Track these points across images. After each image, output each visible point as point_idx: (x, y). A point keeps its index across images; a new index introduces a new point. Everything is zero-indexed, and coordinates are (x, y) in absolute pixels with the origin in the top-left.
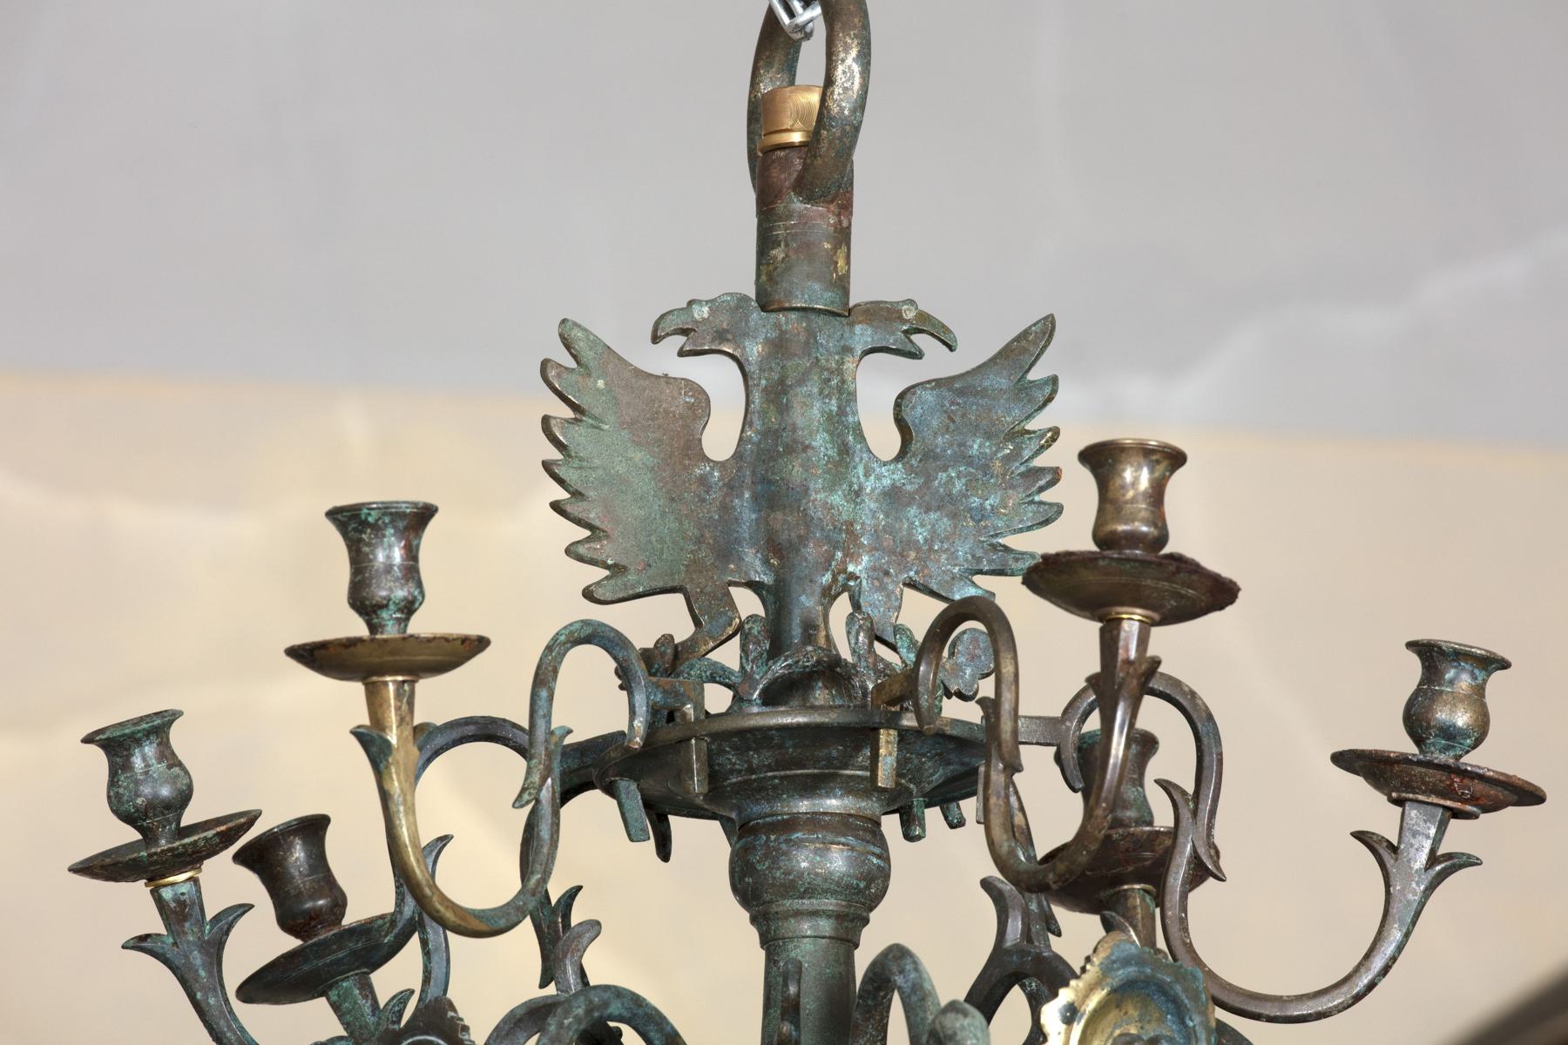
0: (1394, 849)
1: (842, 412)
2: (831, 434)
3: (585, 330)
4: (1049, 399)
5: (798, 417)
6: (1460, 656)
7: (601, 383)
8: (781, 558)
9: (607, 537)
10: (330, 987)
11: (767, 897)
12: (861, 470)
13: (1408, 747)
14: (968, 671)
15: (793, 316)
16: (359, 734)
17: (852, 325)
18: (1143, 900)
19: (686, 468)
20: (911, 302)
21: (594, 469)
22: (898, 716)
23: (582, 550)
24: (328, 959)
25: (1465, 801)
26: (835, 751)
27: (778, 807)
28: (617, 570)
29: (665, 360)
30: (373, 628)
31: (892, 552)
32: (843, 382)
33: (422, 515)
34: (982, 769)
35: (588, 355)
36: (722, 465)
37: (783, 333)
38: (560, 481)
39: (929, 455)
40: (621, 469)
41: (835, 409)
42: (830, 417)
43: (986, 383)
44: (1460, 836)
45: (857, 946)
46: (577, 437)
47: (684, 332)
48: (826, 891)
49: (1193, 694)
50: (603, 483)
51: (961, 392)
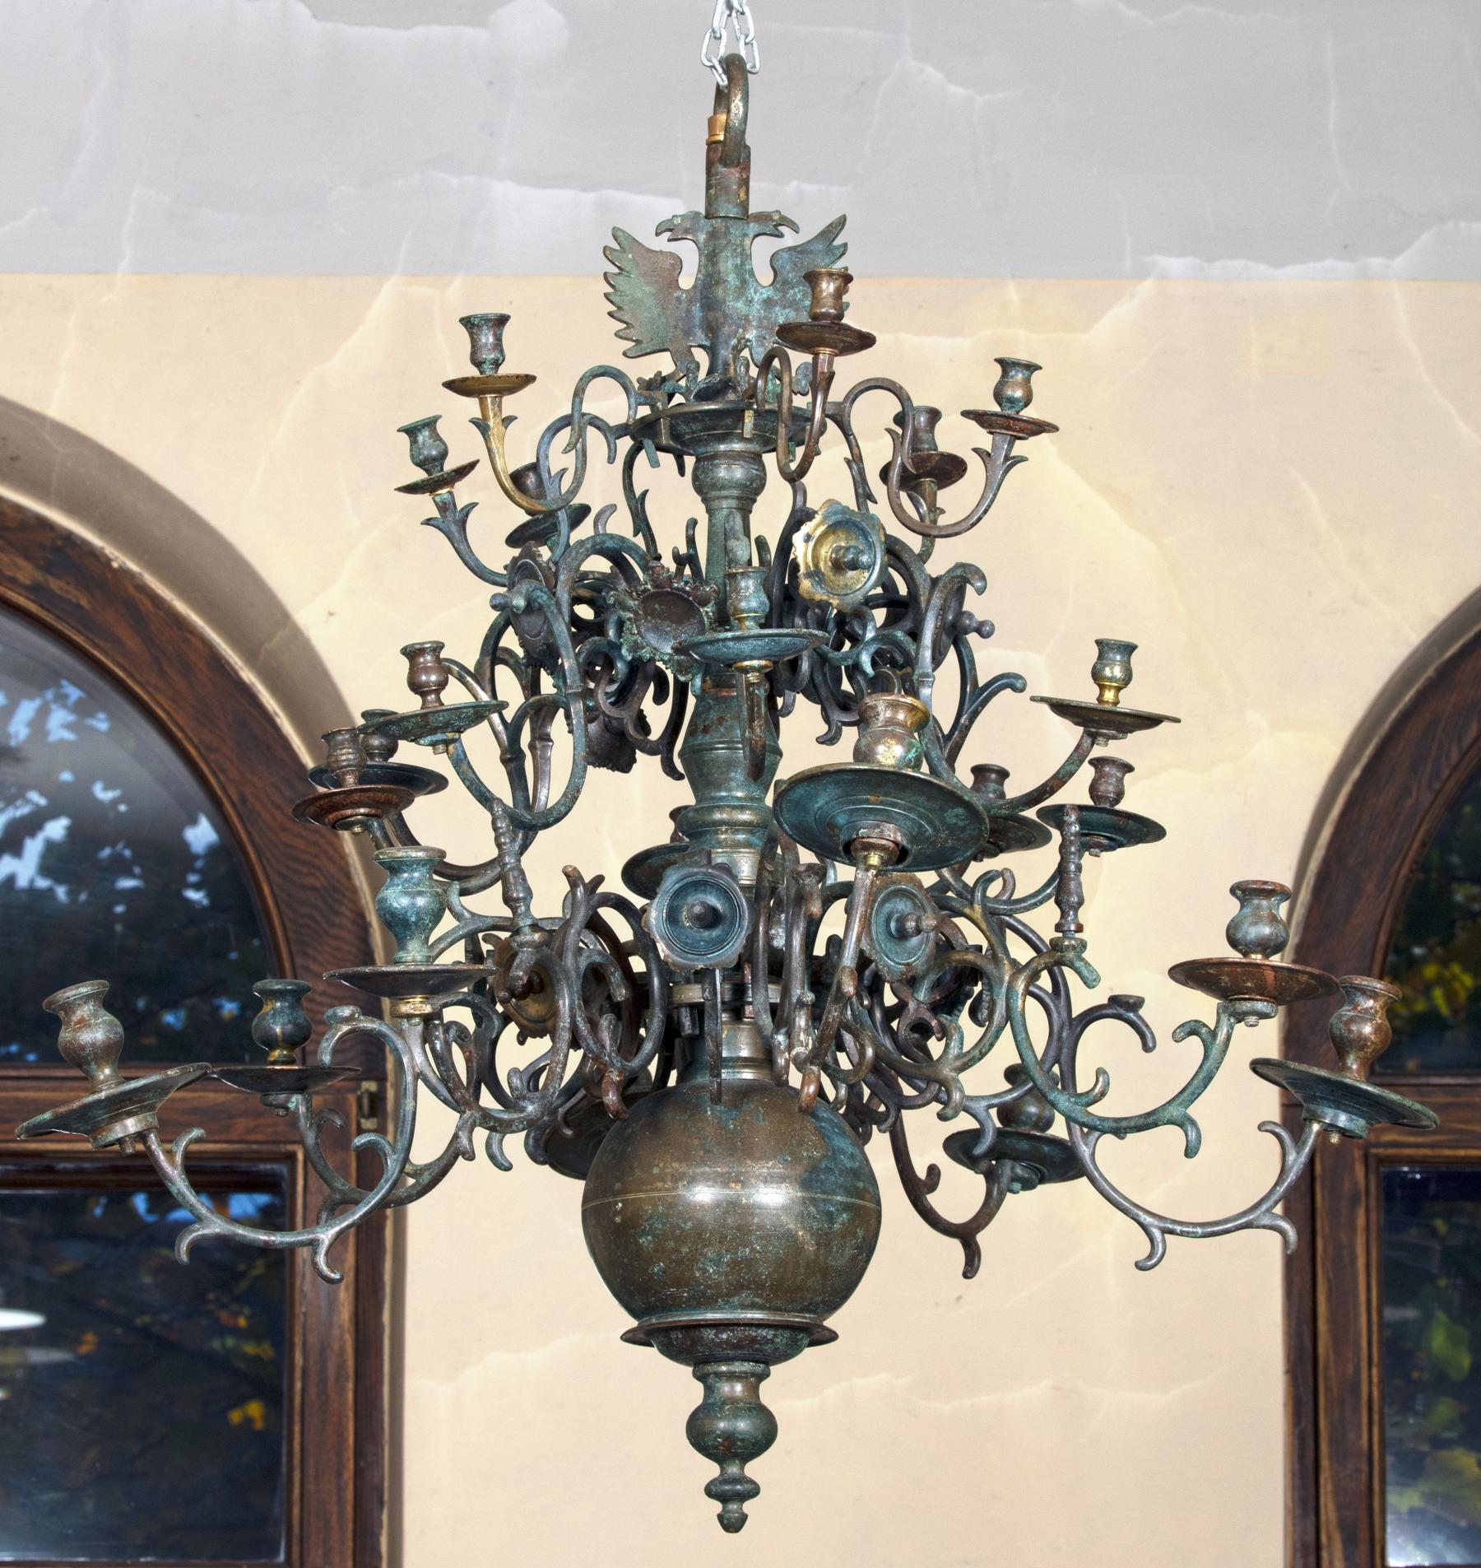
0: (989, 454)
1: (743, 264)
2: (737, 274)
3: (624, 232)
4: (843, 254)
5: (722, 267)
6: (1016, 364)
7: (630, 256)
8: (713, 333)
9: (633, 327)
10: (547, 540)
11: (705, 491)
12: (752, 291)
13: (996, 409)
14: (803, 382)
15: (719, 220)
16: (474, 422)
17: (748, 223)
18: (930, 485)
19: (669, 293)
20: (778, 212)
21: (627, 296)
22: (752, 404)
23: (621, 334)
24: (542, 527)
25: (1018, 432)
26: (729, 421)
27: (709, 449)
28: (638, 342)
29: (661, 244)
30: (481, 373)
31: (766, 328)
32: (744, 250)
33: (502, 320)
34: (808, 427)
35: (625, 243)
36: (687, 291)
37: (715, 228)
38: (612, 302)
39: (785, 282)
40: (640, 295)
41: (739, 262)
42: (736, 266)
43: (812, 248)
44: (1020, 448)
45: (751, 512)
46: (620, 282)
47: (670, 230)
48: (730, 487)
49: (901, 388)
50: (631, 302)
51: (801, 252)
